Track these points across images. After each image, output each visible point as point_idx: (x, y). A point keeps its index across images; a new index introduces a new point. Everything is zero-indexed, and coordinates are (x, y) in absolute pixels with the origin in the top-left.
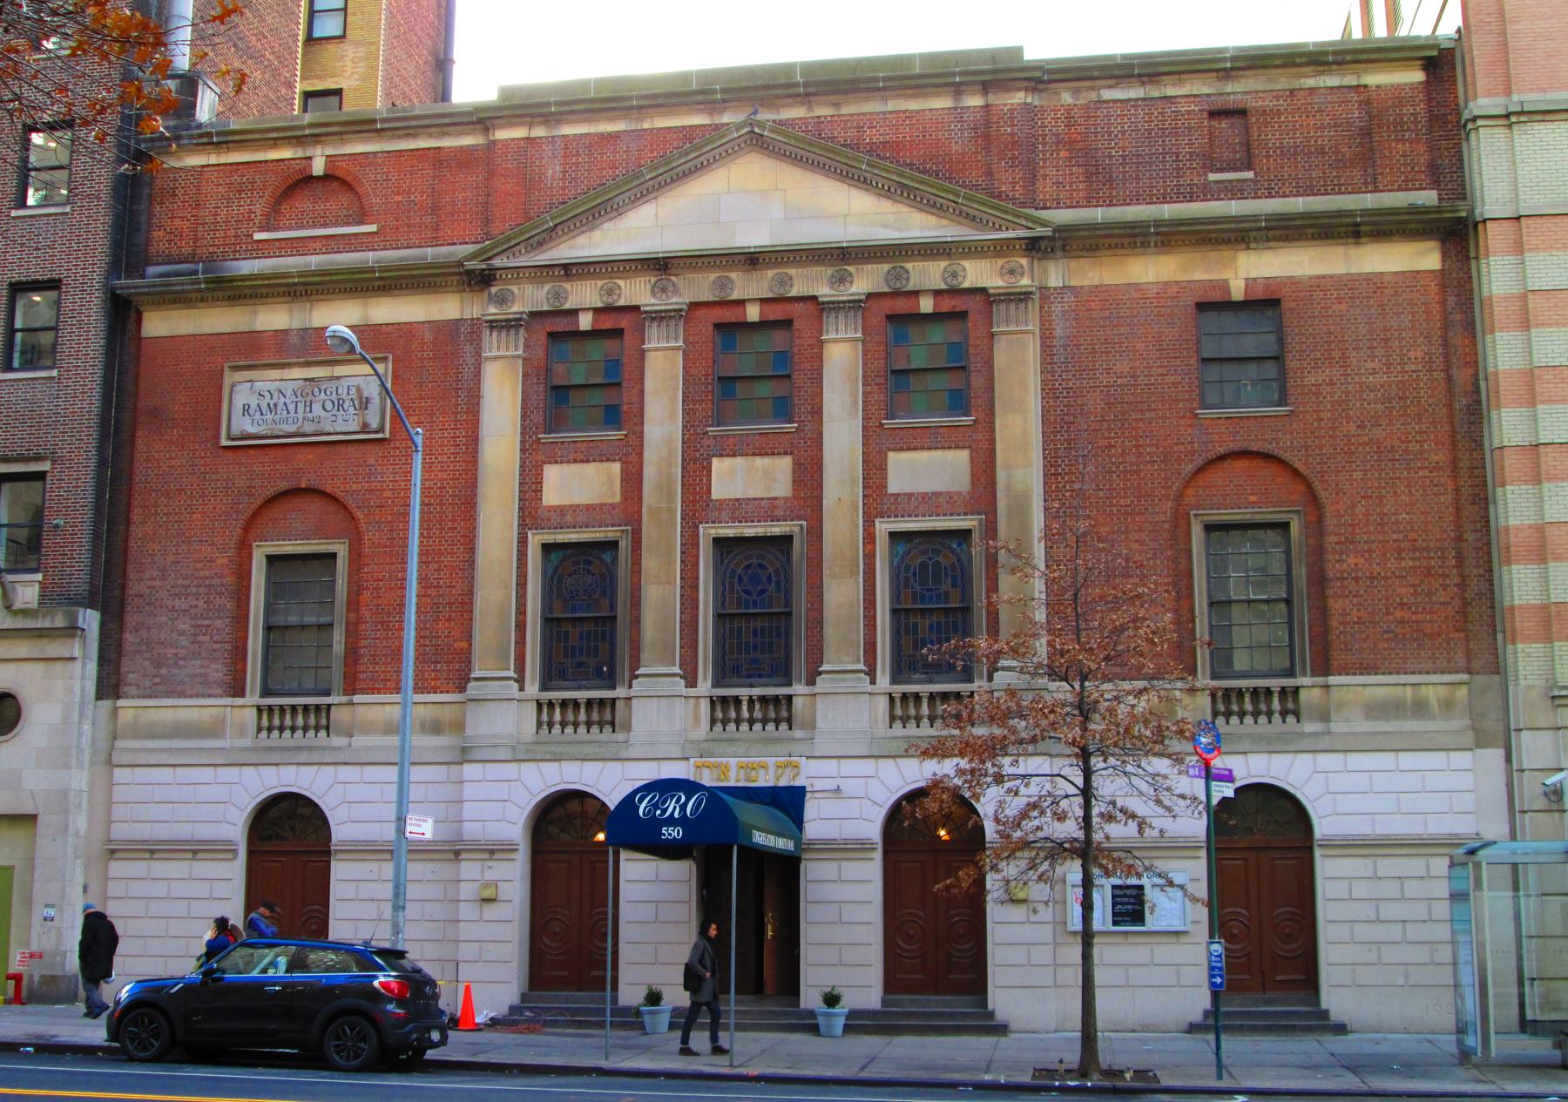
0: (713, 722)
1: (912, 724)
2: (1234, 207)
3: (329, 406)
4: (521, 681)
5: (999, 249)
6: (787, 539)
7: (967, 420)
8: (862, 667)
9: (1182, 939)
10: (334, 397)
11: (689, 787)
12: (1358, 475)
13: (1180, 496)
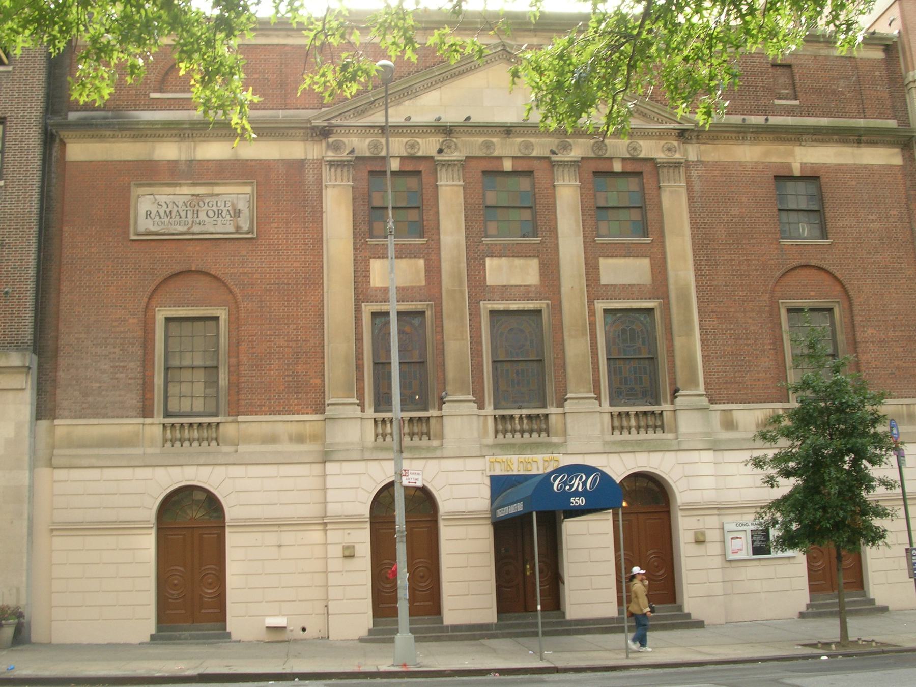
0: (496, 432)
1: (625, 432)
2: (789, 120)
3: (211, 214)
4: (362, 405)
5: (661, 135)
6: (538, 312)
7: (648, 240)
8: (592, 395)
9: (792, 561)
10: (215, 208)
11: (588, 470)
12: (869, 281)
13: (773, 291)
